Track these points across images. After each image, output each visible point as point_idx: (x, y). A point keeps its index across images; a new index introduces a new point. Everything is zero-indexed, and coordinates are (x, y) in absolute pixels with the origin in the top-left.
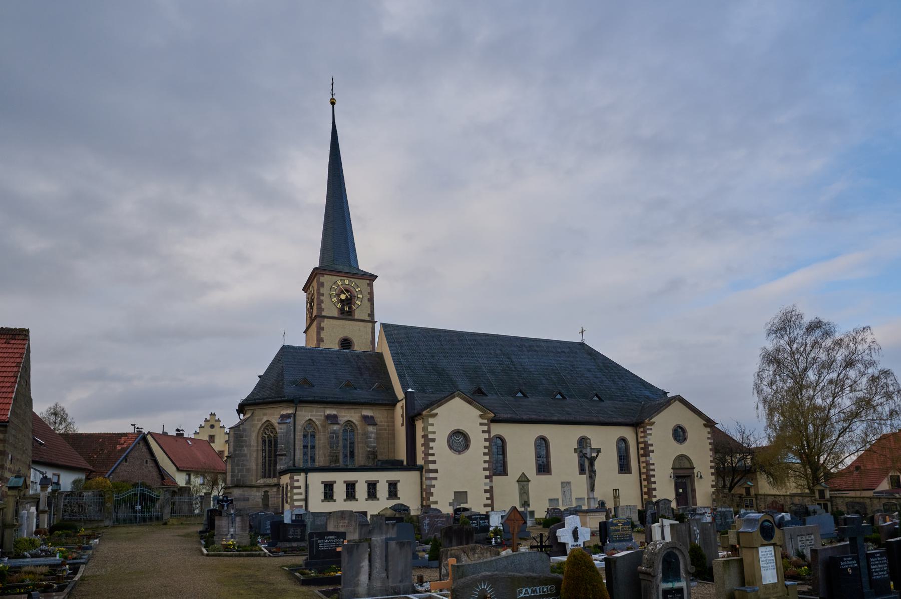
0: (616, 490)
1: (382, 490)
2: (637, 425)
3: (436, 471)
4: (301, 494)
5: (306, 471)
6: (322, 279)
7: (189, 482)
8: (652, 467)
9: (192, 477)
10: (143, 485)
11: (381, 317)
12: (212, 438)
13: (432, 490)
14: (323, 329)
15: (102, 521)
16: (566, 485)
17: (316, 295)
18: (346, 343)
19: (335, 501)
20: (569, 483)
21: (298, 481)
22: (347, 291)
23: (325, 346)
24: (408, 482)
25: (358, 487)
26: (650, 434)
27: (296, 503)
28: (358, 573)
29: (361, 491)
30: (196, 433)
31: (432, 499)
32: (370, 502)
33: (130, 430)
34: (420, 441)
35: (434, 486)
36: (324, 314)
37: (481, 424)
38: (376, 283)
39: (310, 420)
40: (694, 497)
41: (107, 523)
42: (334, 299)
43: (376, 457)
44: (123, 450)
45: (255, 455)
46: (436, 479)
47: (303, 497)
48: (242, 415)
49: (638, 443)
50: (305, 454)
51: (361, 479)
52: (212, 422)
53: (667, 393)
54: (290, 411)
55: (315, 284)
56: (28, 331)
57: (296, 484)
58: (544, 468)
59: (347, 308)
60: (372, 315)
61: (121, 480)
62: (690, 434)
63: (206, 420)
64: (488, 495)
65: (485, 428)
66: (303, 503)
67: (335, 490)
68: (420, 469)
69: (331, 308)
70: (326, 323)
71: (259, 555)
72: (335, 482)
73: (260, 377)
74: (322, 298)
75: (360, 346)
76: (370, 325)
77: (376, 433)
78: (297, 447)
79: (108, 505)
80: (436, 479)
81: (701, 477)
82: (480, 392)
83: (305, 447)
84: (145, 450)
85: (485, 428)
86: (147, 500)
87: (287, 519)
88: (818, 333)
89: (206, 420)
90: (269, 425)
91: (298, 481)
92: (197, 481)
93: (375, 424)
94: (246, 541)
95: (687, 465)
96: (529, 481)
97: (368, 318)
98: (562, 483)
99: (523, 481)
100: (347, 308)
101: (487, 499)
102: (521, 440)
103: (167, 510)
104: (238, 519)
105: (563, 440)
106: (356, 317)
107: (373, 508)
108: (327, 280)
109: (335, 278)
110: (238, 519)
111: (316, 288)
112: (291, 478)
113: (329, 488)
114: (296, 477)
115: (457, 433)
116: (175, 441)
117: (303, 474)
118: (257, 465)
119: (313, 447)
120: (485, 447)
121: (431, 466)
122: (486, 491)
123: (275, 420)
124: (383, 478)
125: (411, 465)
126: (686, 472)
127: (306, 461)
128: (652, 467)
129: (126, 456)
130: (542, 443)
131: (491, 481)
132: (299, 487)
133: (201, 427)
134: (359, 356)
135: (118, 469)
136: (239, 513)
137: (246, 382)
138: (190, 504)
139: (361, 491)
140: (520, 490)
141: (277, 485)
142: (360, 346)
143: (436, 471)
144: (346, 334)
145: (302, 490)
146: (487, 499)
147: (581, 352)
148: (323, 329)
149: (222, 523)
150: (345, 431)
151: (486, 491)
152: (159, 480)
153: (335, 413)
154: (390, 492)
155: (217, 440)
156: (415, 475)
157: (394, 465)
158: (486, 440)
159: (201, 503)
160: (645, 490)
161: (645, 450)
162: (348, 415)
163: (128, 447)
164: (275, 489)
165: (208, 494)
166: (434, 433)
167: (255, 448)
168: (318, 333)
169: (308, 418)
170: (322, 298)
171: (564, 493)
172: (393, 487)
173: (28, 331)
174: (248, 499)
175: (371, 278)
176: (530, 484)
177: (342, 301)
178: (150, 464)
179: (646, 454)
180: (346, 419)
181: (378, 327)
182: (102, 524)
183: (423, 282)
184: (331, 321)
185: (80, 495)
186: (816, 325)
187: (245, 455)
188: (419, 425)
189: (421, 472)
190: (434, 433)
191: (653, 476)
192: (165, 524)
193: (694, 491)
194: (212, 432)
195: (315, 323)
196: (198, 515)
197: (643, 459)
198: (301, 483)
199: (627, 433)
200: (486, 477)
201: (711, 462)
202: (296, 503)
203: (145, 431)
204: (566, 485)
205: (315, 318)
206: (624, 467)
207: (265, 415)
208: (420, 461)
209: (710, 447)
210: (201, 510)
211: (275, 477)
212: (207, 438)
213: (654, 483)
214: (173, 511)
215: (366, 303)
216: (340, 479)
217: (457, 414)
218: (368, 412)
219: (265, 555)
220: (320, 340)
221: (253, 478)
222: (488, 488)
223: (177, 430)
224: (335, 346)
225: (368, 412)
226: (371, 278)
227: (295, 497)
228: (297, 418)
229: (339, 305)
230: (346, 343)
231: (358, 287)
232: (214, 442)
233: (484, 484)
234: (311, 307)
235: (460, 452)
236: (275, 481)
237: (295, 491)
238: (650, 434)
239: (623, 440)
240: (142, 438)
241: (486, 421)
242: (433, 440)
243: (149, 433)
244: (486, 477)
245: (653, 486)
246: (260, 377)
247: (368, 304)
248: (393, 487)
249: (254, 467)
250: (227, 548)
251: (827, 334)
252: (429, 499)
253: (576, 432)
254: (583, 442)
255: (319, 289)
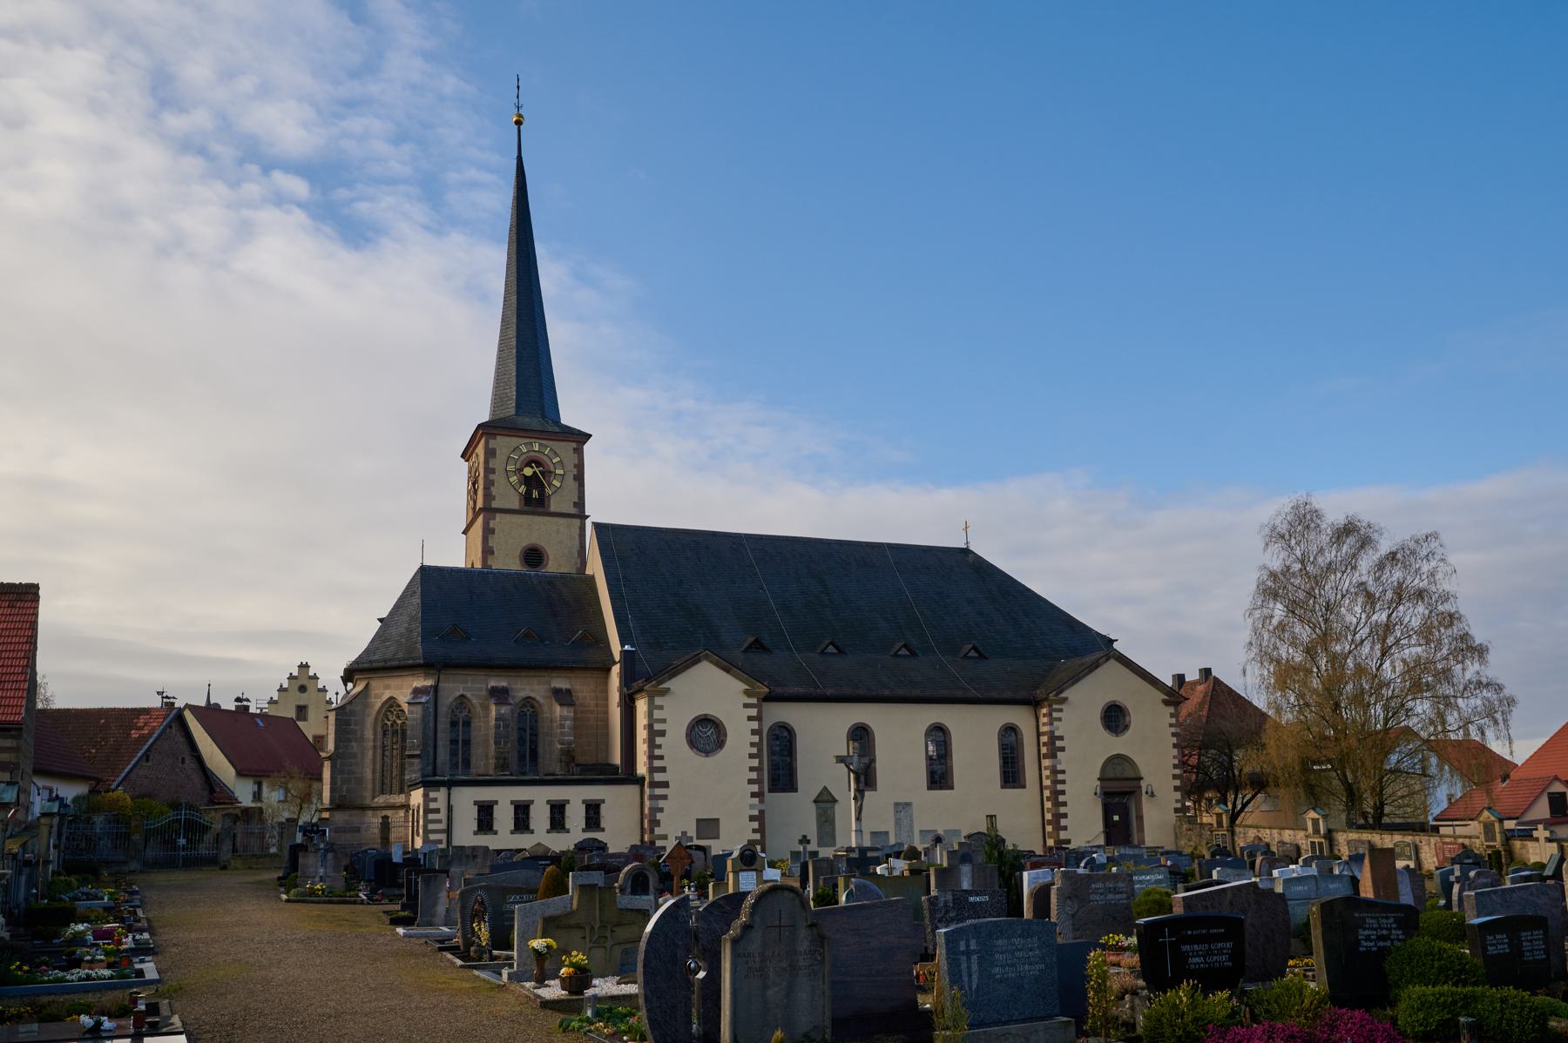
0: (991, 817)
1: (575, 817)
2: (1034, 703)
3: (665, 785)
4: (440, 821)
5: (450, 784)
6: (492, 443)
7: (257, 796)
8: (1060, 777)
9: (265, 789)
10: (190, 807)
11: (598, 511)
12: (302, 711)
13: (659, 816)
14: (492, 531)
15: (125, 863)
16: (902, 808)
17: (481, 470)
18: (533, 556)
19: (532, 832)
20: (908, 804)
21: (435, 800)
22: (539, 464)
23: (498, 564)
24: (619, 803)
25: (568, 810)
26: (1059, 719)
27: (432, 837)
28: (435, 904)
29: (540, 817)
30: (272, 702)
31: (657, 831)
32: (554, 835)
33: (156, 703)
34: (641, 734)
35: (661, 810)
36: (495, 505)
37: (746, 706)
38: (588, 448)
39: (462, 696)
40: (1141, 829)
41: (134, 865)
42: (514, 479)
43: (573, 759)
44: (144, 738)
45: (370, 754)
46: (665, 797)
47: (443, 826)
48: (350, 685)
49: (1039, 734)
50: (453, 753)
51: (540, 798)
52: (303, 681)
53: (1112, 641)
54: (429, 683)
55: (480, 450)
56: (36, 587)
57: (432, 805)
58: (866, 779)
59: (535, 494)
60: (580, 504)
61: (157, 800)
62: (1135, 719)
63: (291, 677)
64: (756, 825)
65: (754, 712)
66: (443, 837)
67: (495, 815)
68: (640, 781)
69: (509, 494)
70: (499, 521)
71: (355, 903)
72: (496, 802)
73: (381, 620)
74: (492, 477)
75: (556, 564)
76: (577, 522)
77: (575, 719)
78: (440, 743)
79: (136, 837)
80: (665, 797)
81: (1152, 795)
82: (758, 646)
83: (454, 742)
84: (181, 739)
85: (754, 712)
86: (195, 829)
87: (397, 857)
88: (1351, 540)
89: (291, 677)
90: (392, 703)
91: (435, 800)
92: (272, 796)
93: (571, 704)
94: (340, 884)
95: (1130, 773)
96: (835, 801)
97: (573, 511)
98: (897, 804)
99: (825, 801)
100: (535, 494)
101: (754, 831)
102: (822, 730)
103: (227, 846)
104: (330, 856)
105: (900, 732)
106: (553, 509)
107: (561, 843)
108: (503, 444)
109: (515, 441)
110: (330, 856)
111: (482, 459)
112: (425, 796)
113: (485, 814)
114: (432, 795)
115: (704, 721)
116: (232, 724)
117: (443, 791)
118: (374, 772)
119: (467, 743)
120: (752, 745)
121: (658, 777)
122: (752, 818)
123: (403, 697)
124: (576, 797)
125: (626, 775)
126: (1126, 786)
127: (454, 766)
128: (1060, 777)
129: (149, 750)
130: (861, 735)
131: (761, 801)
132: (437, 811)
133: (281, 690)
134: (553, 581)
135: (133, 776)
136: (331, 847)
137: (356, 630)
138: (262, 836)
139: (540, 817)
140: (819, 816)
141: (406, 807)
142: (556, 564)
143: (665, 785)
144: (534, 539)
145: (442, 815)
146: (754, 831)
147: (961, 567)
148: (492, 531)
149: (309, 861)
150: (522, 716)
151: (752, 818)
152: (206, 793)
153: (504, 684)
154: (588, 819)
155: (311, 714)
156: (633, 790)
157: (606, 774)
158: (754, 732)
159: (281, 835)
160: (1048, 816)
161: (1053, 747)
162: (528, 688)
163: (150, 735)
164: (402, 813)
165: (292, 821)
166: (664, 721)
167: (371, 744)
168: (485, 540)
169: (458, 694)
170: (492, 477)
171: (898, 822)
172: (593, 813)
173: (36, 587)
174: (358, 830)
175: (580, 438)
176: (837, 806)
177: (527, 481)
178: (190, 764)
179: (1052, 755)
180: (523, 694)
181: (588, 523)
182: (126, 869)
183: (647, 471)
184: (508, 517)
185: (89, 821)
186: (1347, 530)
187: (354, 756)
188: (642, 706)
189: (642, 786)
190: (664, 721)
191: (1063, 792)
192: (224, 868)
193: (1140, 818)
194: (303, 699)
195: (480, 519)
196: (275, 855)
197: (1046, 763)
198: (441, 804)
199: (1020, 717)
200: (753, 795)
201: (1175, 766)
202: (432, 837)
203: (179, 704)
204: (902, 808)
205: (484, 511)
206: (1011, 775)
207: (387, 687)
208: (642, 769)
209: (1174, 740)
210: (280, 848)
211: (401, 791)
212: (292, 714)
213: (1065, 804)
214: (234, 850)
215: (570, 482)
216: (504, 798)
217: (709, 689)
218: (561, 683)
219: (362, 902)
220: (487, 551)
221: (368, 794)
222: (756, 813)
223: (238, 700)
224: (514, 564)
225: (561, 683)
226: (580, 438)
227: (431, 827)
228: (440, 693)
229: (522, 489)
230: (533, 556)
231: (557, 455)
232: (305, 719)
233: (749, 806)
234: (476, 492)
235: (707, 753)
236: (401, 799)
237: (431, 816)
238: (1059, 719)
239: (1010, 730)
240: (173, 717)
241: (754, 701)
242: (662, 733)
243: (187, 706)
244: (753, 795)
245: (1062, 810)
246: (381, 620)
247: (574, 485)
248: (593, 813)
249: (369, 775)
250: (312, 893)
251: (1365, 543)
252: (652, 831)
253: (993, 718)
254: (1010, 730)
255: (486, 462)
